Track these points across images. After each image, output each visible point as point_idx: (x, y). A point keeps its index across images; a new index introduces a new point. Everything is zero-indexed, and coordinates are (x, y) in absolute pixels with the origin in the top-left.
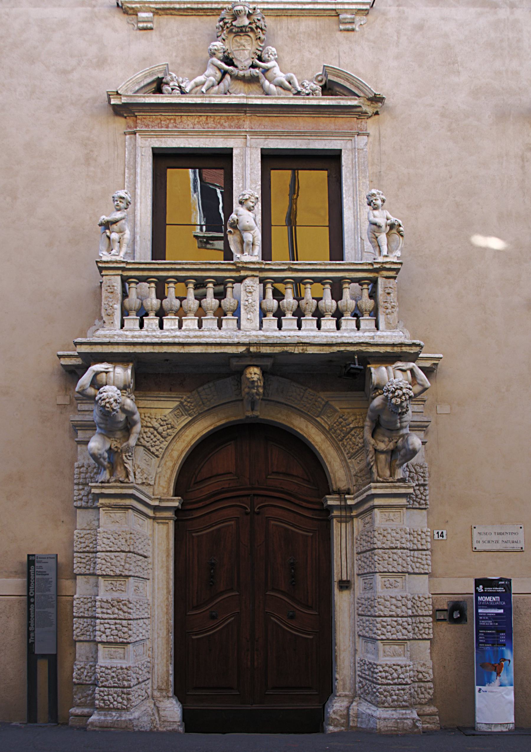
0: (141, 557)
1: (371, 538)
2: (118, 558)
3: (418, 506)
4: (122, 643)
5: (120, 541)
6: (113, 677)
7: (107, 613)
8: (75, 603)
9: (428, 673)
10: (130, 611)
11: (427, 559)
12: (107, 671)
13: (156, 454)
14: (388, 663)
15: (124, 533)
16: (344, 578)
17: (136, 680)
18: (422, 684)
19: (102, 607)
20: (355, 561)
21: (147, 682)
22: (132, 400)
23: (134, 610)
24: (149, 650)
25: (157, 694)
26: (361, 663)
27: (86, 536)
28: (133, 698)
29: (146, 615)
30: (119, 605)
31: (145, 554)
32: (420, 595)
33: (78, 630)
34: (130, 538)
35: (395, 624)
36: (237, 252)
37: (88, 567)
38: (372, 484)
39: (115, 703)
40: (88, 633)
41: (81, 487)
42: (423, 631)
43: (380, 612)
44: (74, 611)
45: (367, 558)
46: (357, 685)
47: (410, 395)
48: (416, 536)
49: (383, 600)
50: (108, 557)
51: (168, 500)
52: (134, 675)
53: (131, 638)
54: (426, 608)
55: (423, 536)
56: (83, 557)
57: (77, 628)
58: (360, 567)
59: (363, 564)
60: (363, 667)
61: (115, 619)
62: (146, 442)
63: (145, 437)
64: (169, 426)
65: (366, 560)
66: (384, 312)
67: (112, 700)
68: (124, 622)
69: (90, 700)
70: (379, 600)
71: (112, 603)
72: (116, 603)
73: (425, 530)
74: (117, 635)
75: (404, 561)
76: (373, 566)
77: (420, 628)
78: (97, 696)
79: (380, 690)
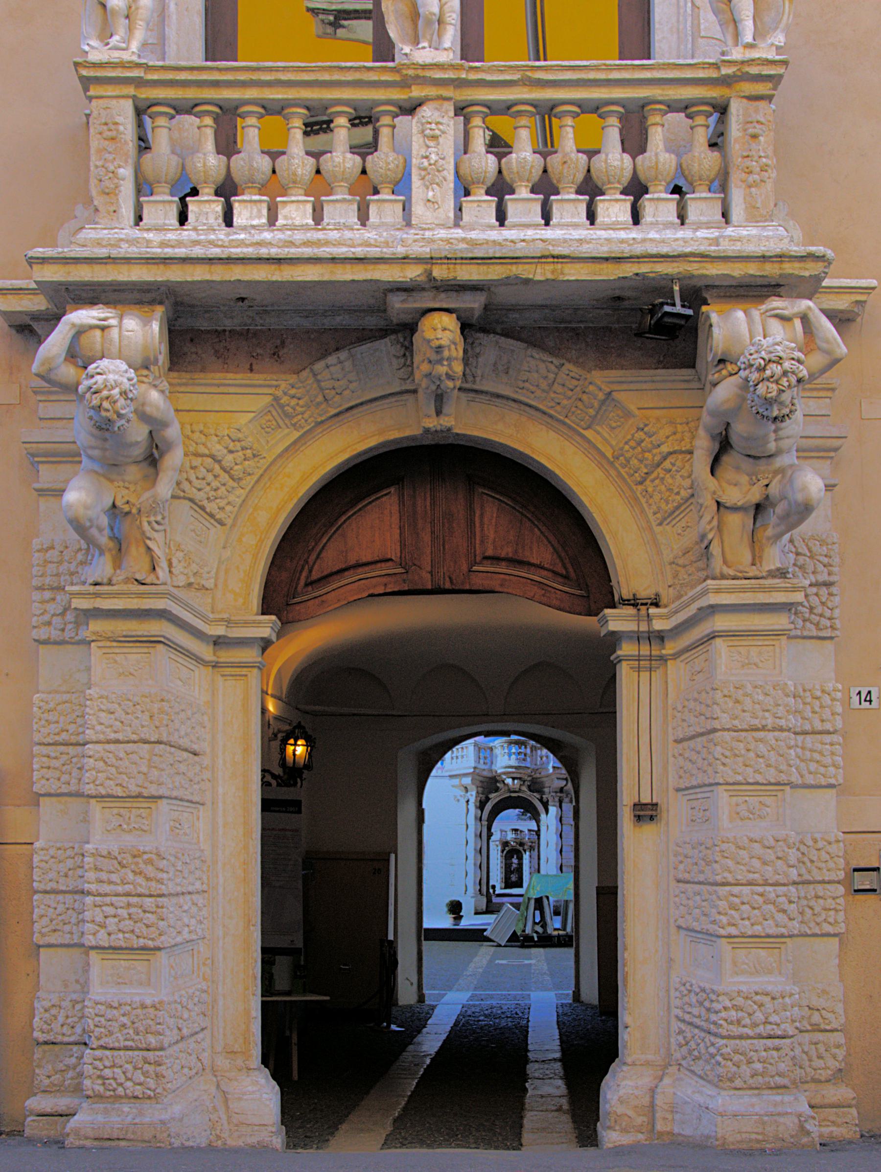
0: (185, 755)
1: (708, 706)
2: (135, 757)
3: (814, 633)
4: (144, 948)
5: (137, 718)
6: (124, 1026)
7: (110, 882)
8: (36, 859)
9: (833, 1012)
10: (161, 875)
11: (833, 754)
12: (110, 1013)
13: (218, 517)
14: (744, 988)
15: (148, 700)
16: (645, 799)
17: (176, 1031)
18: (820, 1036)
19: (97, 869)
20: (671, 760)
21: (201, 1035)
22: (163, 392)
23: (171, 875)
24: (204, 964)
25: (222, 1062)
26: (682, 988)
27: (59, 707)
28: (169, 1074)
29: (198, 886)
30: (137, 864)
31: (196, 747)
32: (818, 836)
33: (45, 921)
34: (161, 711)
35: (760, 900)
36: (403, 43)
37: (65, 778)
38: (709, 582)
39: (129, 1084)
40: (67, 928)
41: (48, 595)
42: (824, 916)
43: (726, 874)
44: (35, 877)
45: (699, 753)
46: (672, 1040)
47: (800, 375)
48: (809, 700)
49: (733, 848)
50: (111, 755)
51: (246, 624)
52: (171, 1022)
53: (163, 938)
54: (831, 865)
55: (827, 700)
56: (53, 754)
57: (42, 916)
58: (681, 772)
59: (689, 765)
60: (686, 999)
61: (128, 894)
62: (195, 490)
63: (193, 478)
64: (249, 452)
65: (694, 757)
66: (742, 181)
67: (122, 1079)
68: (148, 902)
69: (72, 1078)
70: (724, 846)
71: (119, 859)
72: (130, 859)
73: (829, 686)
74: (133, 931)
75: (780, 759)
76: (710, 770)
77: (817, 909)
78: (88, 1069)
79: (724, 1050)
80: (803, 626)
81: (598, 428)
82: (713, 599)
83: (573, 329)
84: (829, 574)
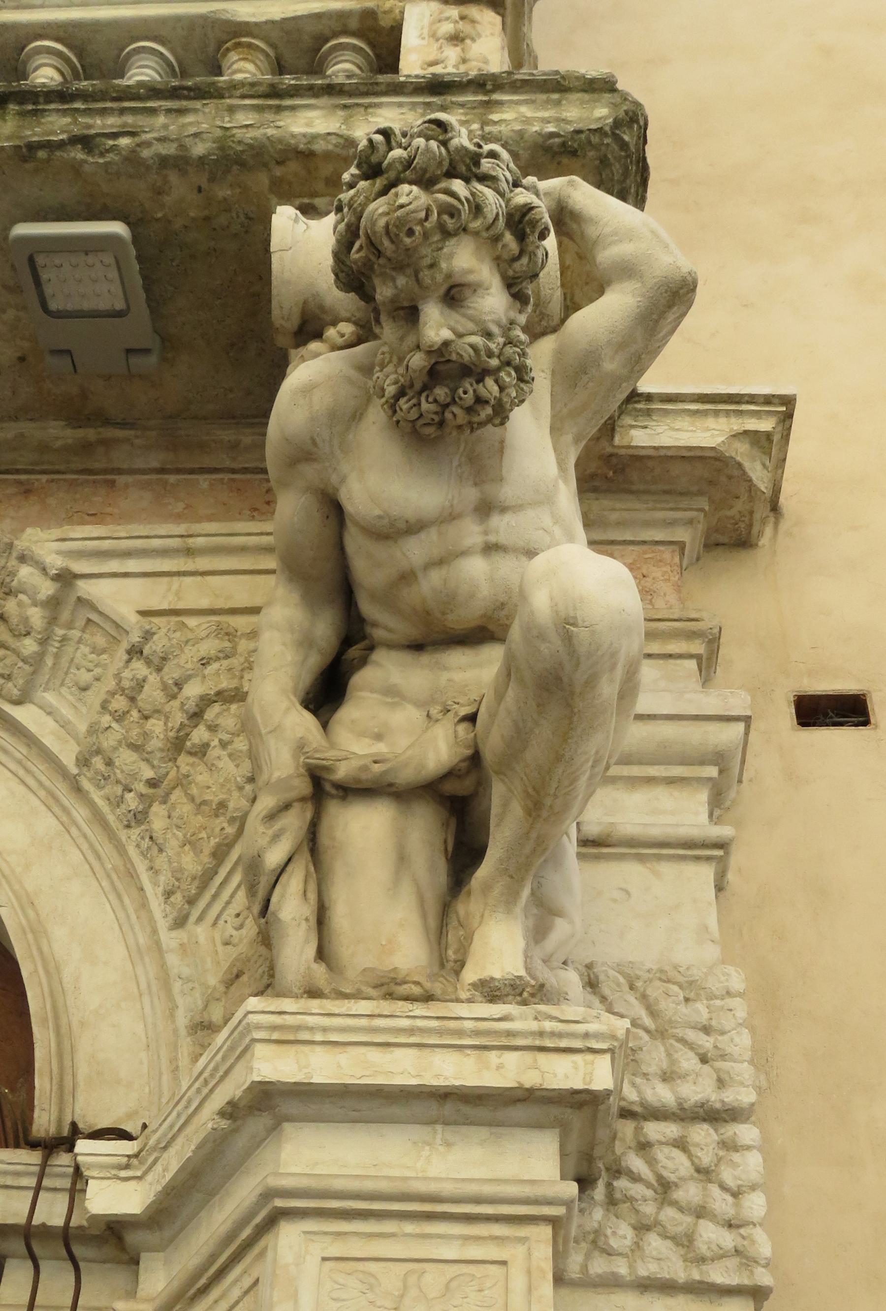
3: (677, 1269)
80: (637, 1246)
81: (50, 697)
82: (273, 1065)
83: (19, 483)
84: (721, 1083)
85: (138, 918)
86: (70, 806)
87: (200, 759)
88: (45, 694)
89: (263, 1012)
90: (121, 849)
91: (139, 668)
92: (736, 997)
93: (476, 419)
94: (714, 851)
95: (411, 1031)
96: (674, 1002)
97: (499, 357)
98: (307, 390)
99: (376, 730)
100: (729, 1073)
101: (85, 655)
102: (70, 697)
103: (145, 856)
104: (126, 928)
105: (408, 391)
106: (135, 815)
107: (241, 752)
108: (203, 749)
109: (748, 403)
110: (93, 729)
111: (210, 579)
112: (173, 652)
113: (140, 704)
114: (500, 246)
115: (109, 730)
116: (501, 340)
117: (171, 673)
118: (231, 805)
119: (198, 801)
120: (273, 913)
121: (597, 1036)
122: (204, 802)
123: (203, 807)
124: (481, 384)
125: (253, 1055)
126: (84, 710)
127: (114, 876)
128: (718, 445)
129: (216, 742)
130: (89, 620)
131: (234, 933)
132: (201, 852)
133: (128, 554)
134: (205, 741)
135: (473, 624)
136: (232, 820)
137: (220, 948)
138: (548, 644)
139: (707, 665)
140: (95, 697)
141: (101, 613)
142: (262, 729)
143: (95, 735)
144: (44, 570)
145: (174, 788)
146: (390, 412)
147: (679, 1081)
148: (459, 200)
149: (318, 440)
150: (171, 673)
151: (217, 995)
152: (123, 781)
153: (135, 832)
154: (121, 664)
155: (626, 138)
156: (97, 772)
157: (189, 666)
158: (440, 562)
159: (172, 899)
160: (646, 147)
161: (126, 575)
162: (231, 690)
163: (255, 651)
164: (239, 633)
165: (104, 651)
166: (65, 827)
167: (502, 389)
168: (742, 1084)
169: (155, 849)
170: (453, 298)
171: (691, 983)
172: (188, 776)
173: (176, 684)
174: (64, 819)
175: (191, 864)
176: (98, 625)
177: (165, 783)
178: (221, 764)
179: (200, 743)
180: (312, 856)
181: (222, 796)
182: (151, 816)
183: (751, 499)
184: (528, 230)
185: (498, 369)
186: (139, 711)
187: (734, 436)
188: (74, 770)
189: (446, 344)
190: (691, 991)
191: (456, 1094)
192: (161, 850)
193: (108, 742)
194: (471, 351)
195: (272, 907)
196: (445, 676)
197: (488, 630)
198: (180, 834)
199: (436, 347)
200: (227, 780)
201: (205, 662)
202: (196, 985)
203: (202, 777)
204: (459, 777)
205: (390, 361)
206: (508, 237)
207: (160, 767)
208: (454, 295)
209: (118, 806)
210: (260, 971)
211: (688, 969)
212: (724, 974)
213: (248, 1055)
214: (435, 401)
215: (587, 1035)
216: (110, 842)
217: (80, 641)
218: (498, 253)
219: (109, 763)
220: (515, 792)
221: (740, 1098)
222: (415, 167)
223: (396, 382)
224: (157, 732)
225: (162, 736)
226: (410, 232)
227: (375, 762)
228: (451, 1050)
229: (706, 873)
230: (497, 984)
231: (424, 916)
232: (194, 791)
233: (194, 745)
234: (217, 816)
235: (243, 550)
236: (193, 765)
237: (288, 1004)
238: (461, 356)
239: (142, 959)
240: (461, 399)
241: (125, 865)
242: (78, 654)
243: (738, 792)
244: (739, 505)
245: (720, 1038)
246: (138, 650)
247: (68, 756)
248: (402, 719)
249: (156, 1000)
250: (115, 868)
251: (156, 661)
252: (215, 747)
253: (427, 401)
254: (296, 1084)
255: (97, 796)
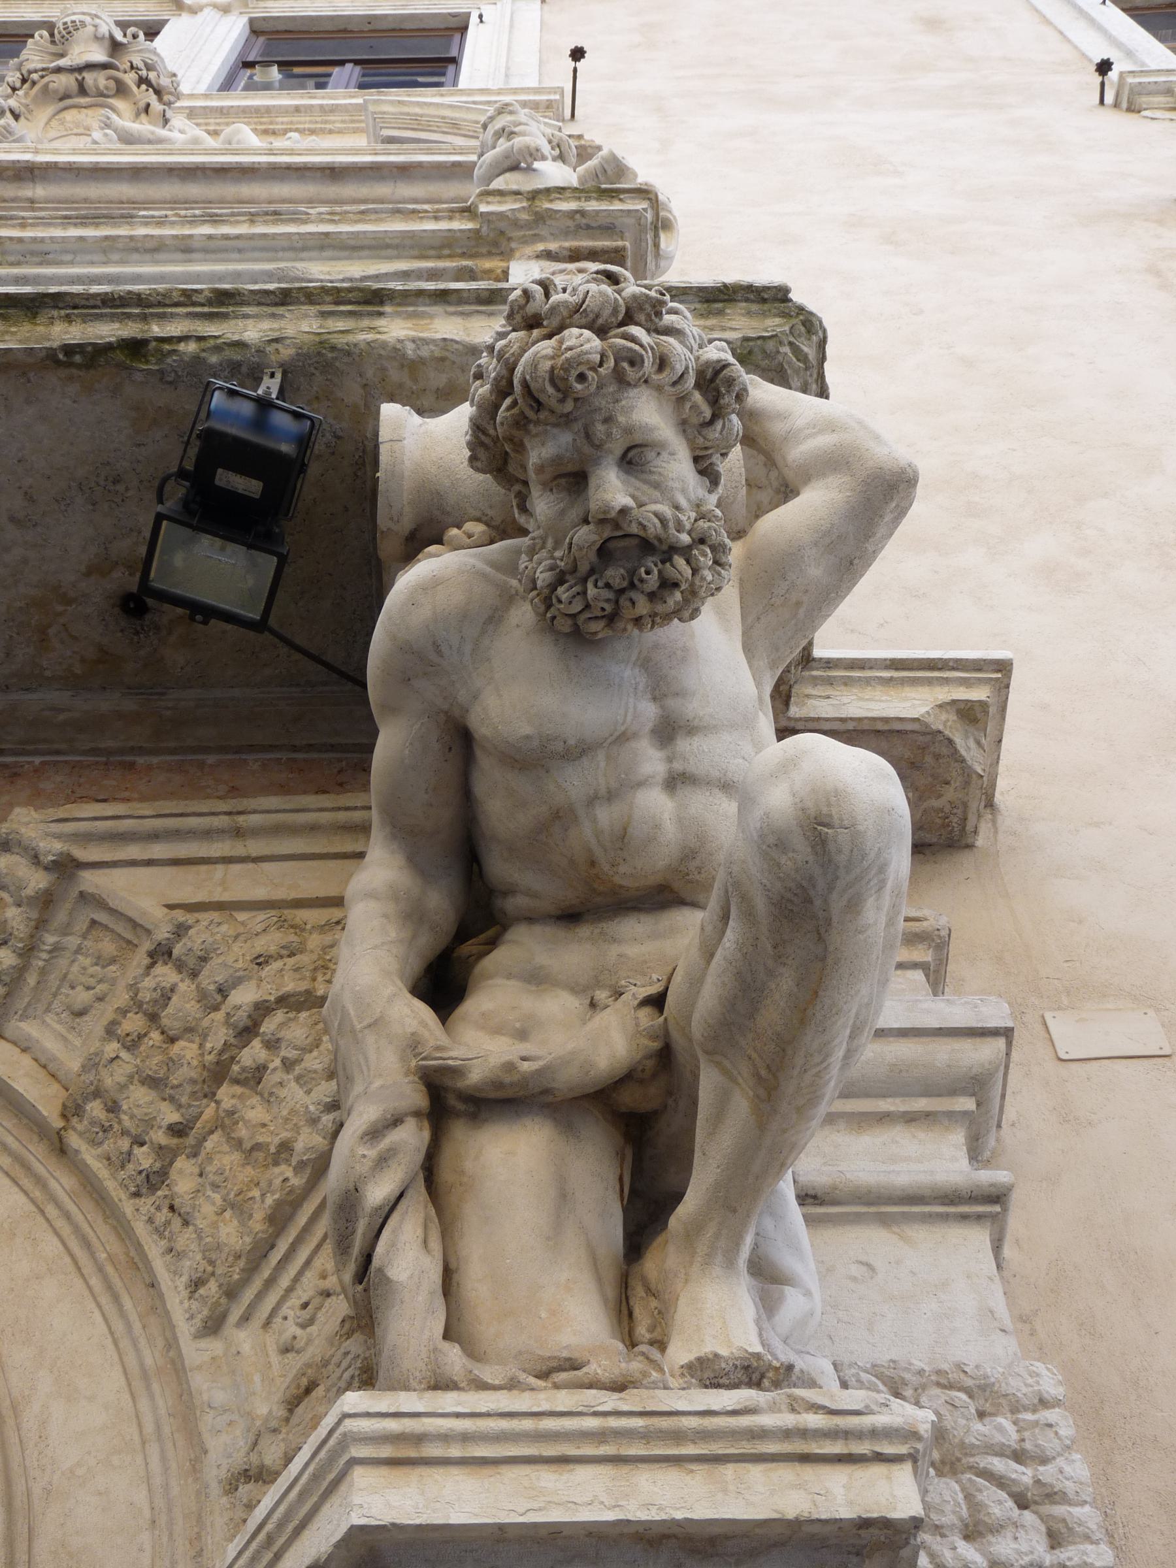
81: (30, 1028)
85: (144, 1327)
86: (47, 1175)
87: (252, 1089)
88: (22, 1025)
89: (368, 1415)
90: (123, 1229)
91: (165, 974)
92: (1053, 1407)
93: (660, 608)
94: (985, 1205)
95: (601, 1436)
96: (964, 1416)
97: (689, 533)
98: (431, 585)
99: (518, 1025)
100: (1064, 1520)
101: (84, 968)
102: (58, 1027)
103: (161, 1235)
104: (125, 1343)
105: (568, 577)
106: (148, 1176)
107: (315, 1072)
108: (257, 1075)
109: (953, 669)
110: (92, 1063)
111: (266, 866)
112: (215, 949)
113: (165, 1021)
114: (688, 405)
115: (115, 1062)
116: (693, 515)
117: (211, 976)
118: (299, 1146)
119: (247, 1145)
120: (380, 1270)
121: (888, 1434)
122: (257, 1147)
123: (255, 1154)
124: (668, 564)
125: (351, 1485)
126: (77, 1042)
127: (110, 1270)
128: (922, 716)
129: (277, 1062)
130: (94, 922)
131: (299, 1332)
132: (251, 1216)
133: (154, 836)
134: (262, 1061)
135: (652, 880)
136: (300, 1167)
137: (275, 1358)
138: (791, 855)
139: (936, 977)
140: (95, 1024)
141: (113, 911)
142: (356, 1023)
143: (94, 1071)
144: (36, 860)
145: (212, 1132)
146: (542, 608)
147: (990, 1538)
148: (642, 346)
149: (444, 648)
150: (211, 976)
151: (274, 1424)
152: (133, 1131)
153: (146, 1204)
154: (140, 971)
155: (806, 349)
156: (93, 1123)
157: (240, 965)
158: (611, 796)
159: (202, 1291)
160: (825, 364)
161: (150, 863)
162: (300, 994)
163: (332, 946)
164: (308, 927)
165: (113, 961)
166: (38, 1207)
167: (695, 572)
168: (1087, 1538)
169: (177, 1222)
170: (630, 463)
171: (983, 1388)
172: (233, 1113)
173: (220, 990)
174: (37, 1194)
175: (232, 1234)
176: (106, 927)
177: (198, 1125)
178: (283, 1093)
179: (254, 1066)
180: (430, 1194)
181: (285, 1135)
182: (173, 1174)
183: (967, 783)
184: (723, 390)
185: (690, 547)
186: (163, 1033)
187: (940, 706)
188: (58, 1123)
189: (624, 511)
190: (986, 1400)
191: (675, 1536)
192: (186, 1223)
193: (111, 1079)
194: (656, 521)
195: (376, 1262)
196: (614, 951)
197: (672, 891)
198: (217, 1197)
199: (613, 514)
200: (293, 1111)
201: (261, 961)
202: (235, 1417)
203: (255, 1112)
204: (641, 1081)
205: (543, 547)
206: (697, 397)
207: (190, 1106)
208: (634, 459)
209: (123, 1167)
210: (347, 1375)
211: (977, 1367)
212: (1032, 1374)
213: (343, 1487)
214: (608, 586)
215: (874, 1434)
216: (106, 1223)
217: (78, 951)
218: (684, 416)
219: (113, 1108)
220: (740, 1081)
221: (1089, 1560)
222: (585, 310)
223: (551, 569)
224: (188, 1057)
225: (195, 1063)
226: (582, 377)
227: (524, 1059)
228: (664, 1465)
229: (978, 1238)
230: (723, 1365)
231: (599, 1280)
232: (242, 1132)
233: (244, 1069)
234: (276, 1163)
235: (313, 829)
236: (241, 1097)
237: (408, 1401)
238: (644, 527)
239: (148, 1387)
240: (642, 581)
241: (127, 1254)
242: (75, 968)
243: (997, 1140)
244: (950, 793)
245: (1041, 1468)
246: (164, 949)
247: (50, 1112)
248: (549, 1014)
249: (169, 1445)
250: (110, 1257)
251: (191, 962)
252: (275, 1069)
253: (596, 586)
254: (419, 1527)
255: (91, 1157)
